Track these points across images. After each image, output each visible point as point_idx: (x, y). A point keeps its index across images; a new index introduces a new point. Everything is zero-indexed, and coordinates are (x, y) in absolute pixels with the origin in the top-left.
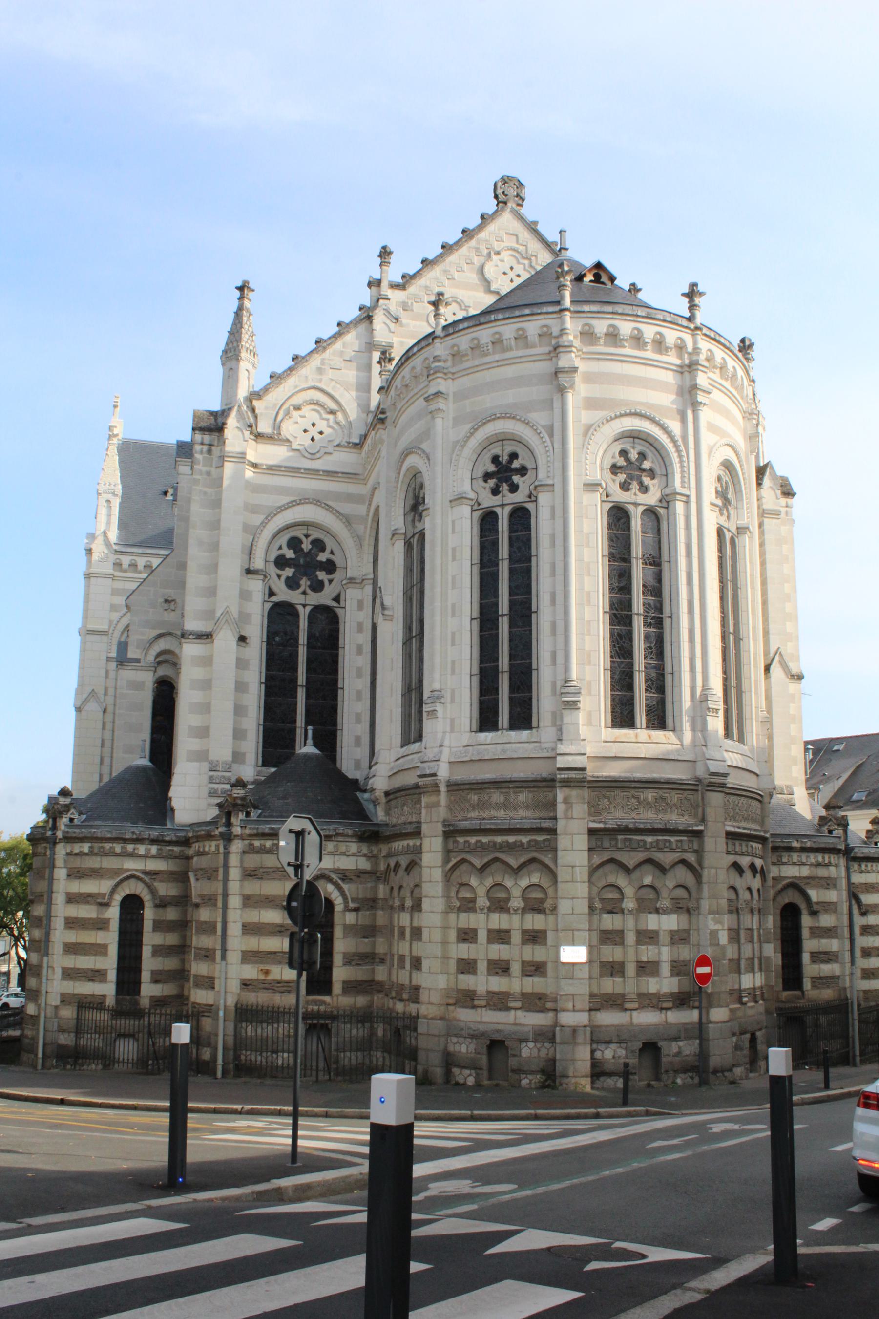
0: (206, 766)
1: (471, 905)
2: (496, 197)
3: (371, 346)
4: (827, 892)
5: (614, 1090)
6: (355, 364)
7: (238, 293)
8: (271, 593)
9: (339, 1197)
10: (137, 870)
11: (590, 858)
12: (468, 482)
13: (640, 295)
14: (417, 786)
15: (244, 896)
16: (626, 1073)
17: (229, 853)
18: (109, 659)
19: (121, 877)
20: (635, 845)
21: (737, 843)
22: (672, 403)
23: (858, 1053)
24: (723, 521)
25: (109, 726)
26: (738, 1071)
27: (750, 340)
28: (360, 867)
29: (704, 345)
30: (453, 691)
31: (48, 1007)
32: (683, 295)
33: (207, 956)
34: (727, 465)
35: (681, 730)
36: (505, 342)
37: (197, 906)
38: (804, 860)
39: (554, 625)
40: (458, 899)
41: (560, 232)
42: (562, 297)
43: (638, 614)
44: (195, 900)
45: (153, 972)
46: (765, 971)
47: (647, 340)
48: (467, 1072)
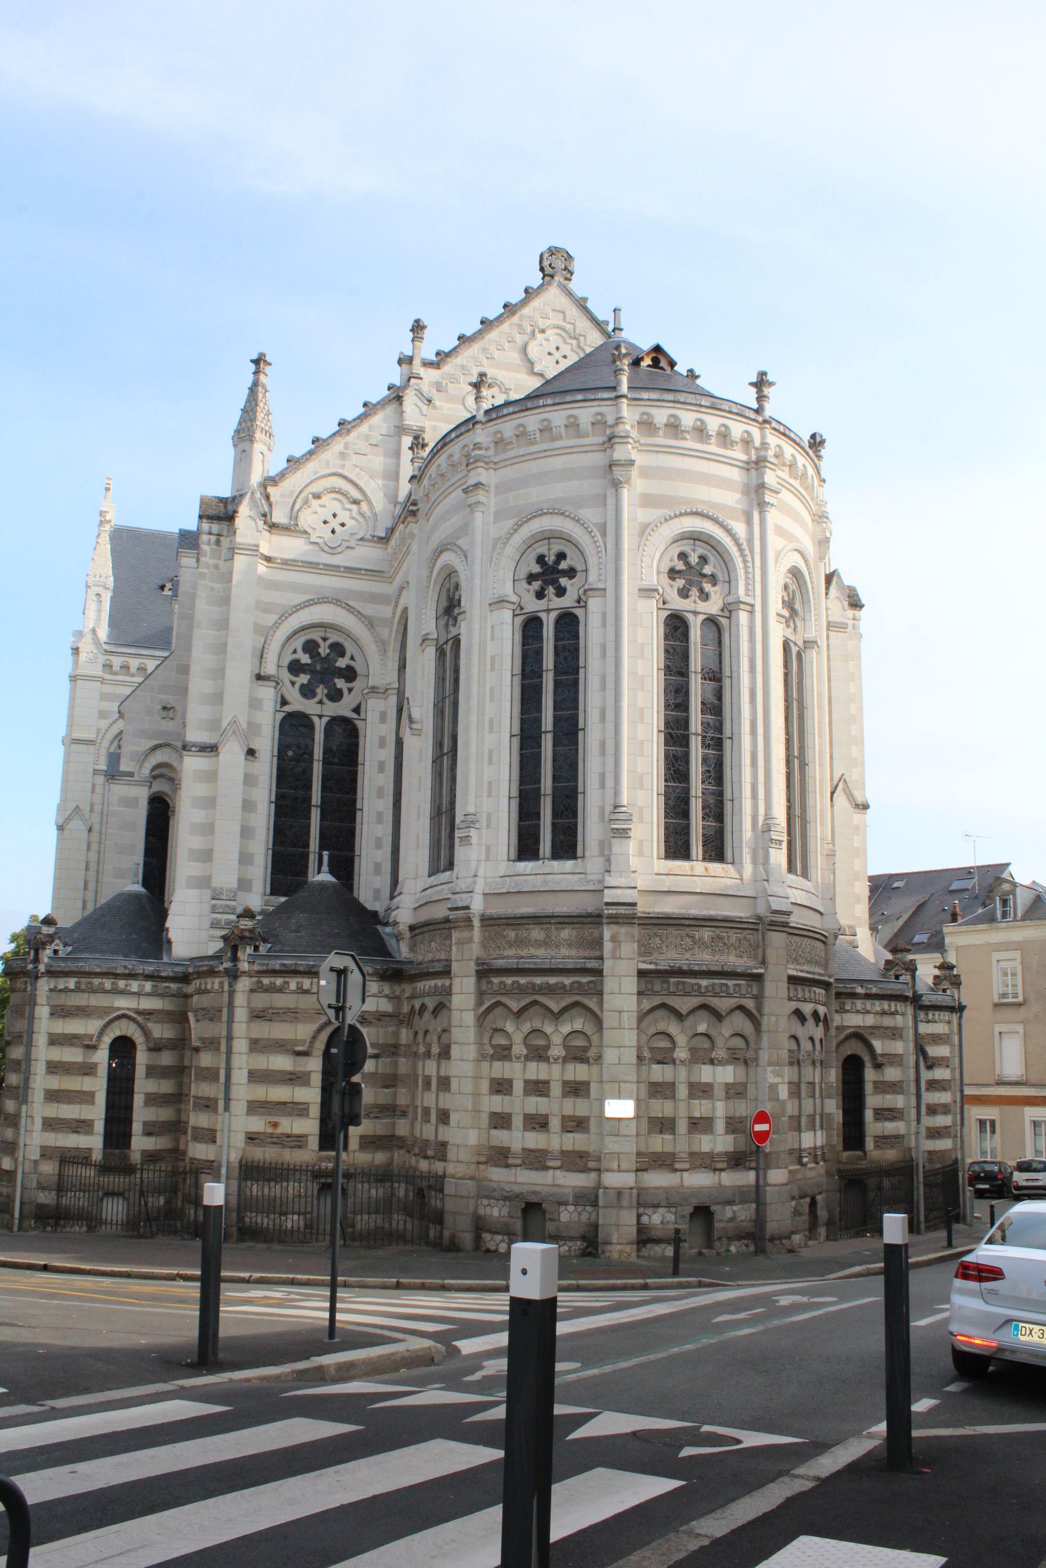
0: (207, 894)
1: (506, 1053)
2: (542, 269)
3: (401, 429)
4: (893, 1042)
5: (664, 1258)
6: (382, 450)
7: (252, 367)
8: (284, 702)
9: (386, 1376)
10: (129, 1009)
11: (639, 1003)
13: (698, 382)
14: (447, 920)
16: (677, 1240)
17: (234, 991)
18: (96, 772)
19: (111, 1017)
20: (688, 989)
21: (800, 988)
22: (737, 502)
23: (922, 1219)
24: (789, 633)
25: (95, 847)
26: (797, 1238)
27: (821, 436)
28: (381, 1009)
29: (773, 440)
30: (489, 815)
31: (27, 1162)
32: (751, 384)
33: (208, 1107)
34: (795, 573)
35: (741, 863)
36: (554, 429)
37: (197, 1050)
38: (868, 1008)
40: (491, 1045)
41: (615, 311)
42: (619, 382)
43: (696, 734)
44: (195, 1043)
45: (146, 1124)
46: (827, 1130)
47: (710, 433)
48: (499, 1238)
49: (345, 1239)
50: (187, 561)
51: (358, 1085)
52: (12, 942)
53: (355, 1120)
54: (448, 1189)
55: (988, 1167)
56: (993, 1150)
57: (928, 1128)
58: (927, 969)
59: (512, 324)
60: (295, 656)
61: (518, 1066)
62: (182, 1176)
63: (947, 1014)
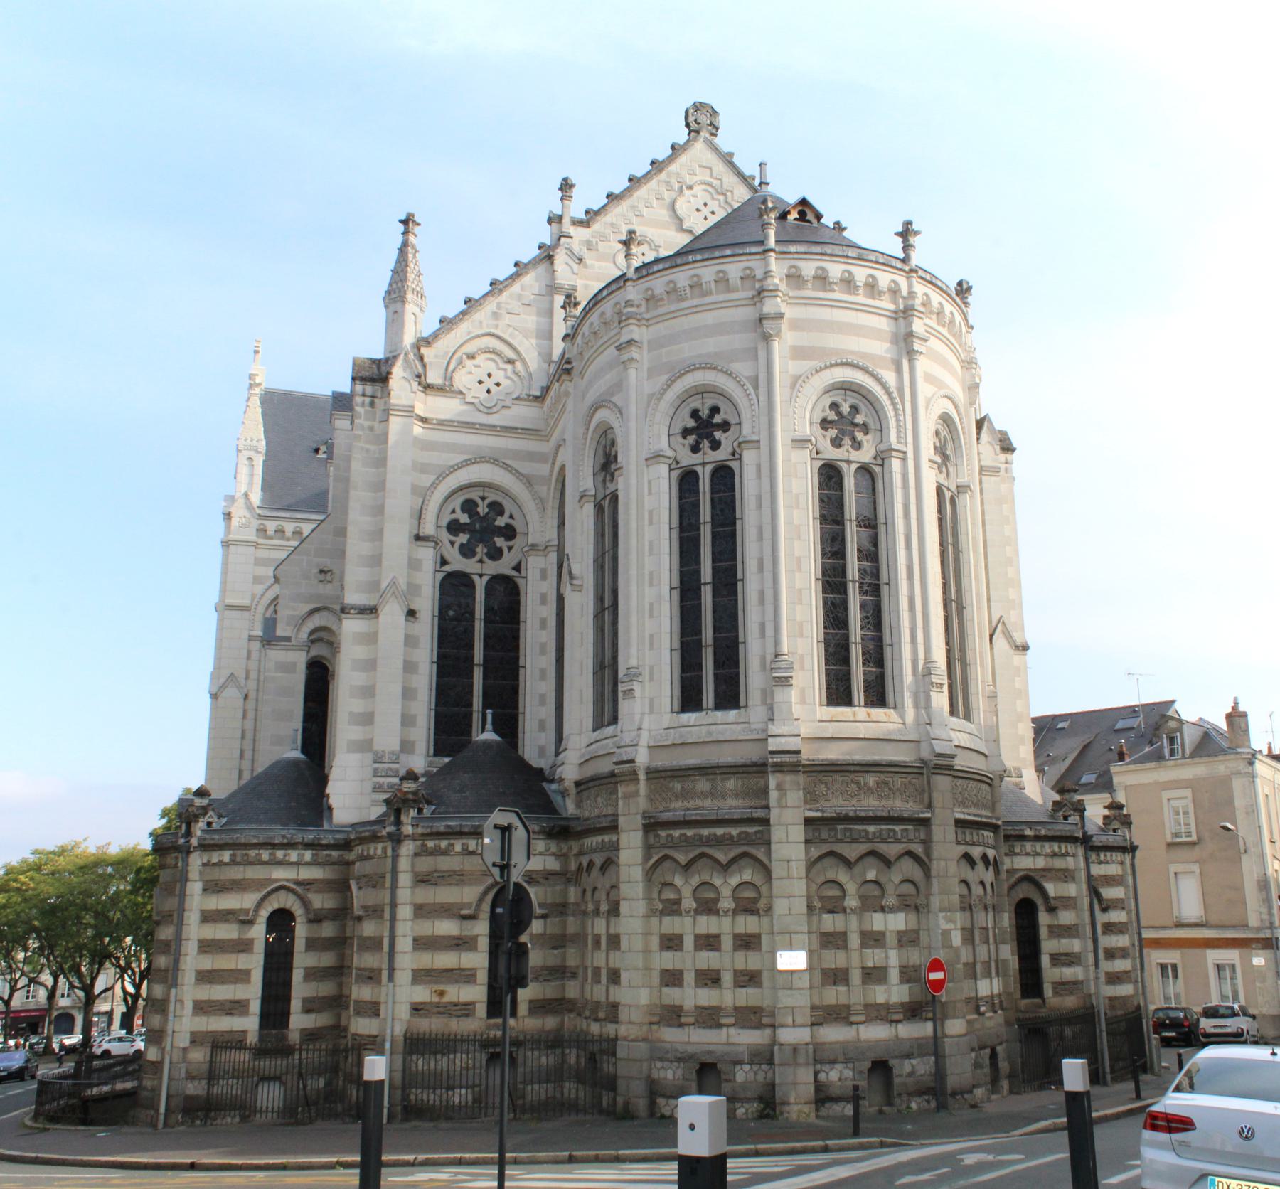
0: (369, 757)
1: (675, 907)
2: (688, 125)
3: (552, 288)
5: (843, 1118)
7: (401, 228)
8: (444, 562)
10: (287, 880)
11: (807, 852)
12: (665, 439)
13: (845, 234)
14: (612, 774)
15: (415, 905)
16: (855, 1097)
18: (251, 638)
21: (967, 831)
23: (1108, 1069)
24: (942, 479)
25: (251, 715)
26: (979, 1092)
29: (920, 289)
32: (897, 234)
33: (371, 978)
34: (946, 419)
37: (359, 919)
38: (1038, 850)
39: (762, 593)
42: (766, 237)
43: (854, 581)
44: (357, 911)
49: (515, 1111)
50: (342, 423)
51: (525, 944)
52: (163, 817)
53: (521, 981)
54: (621, 1053)
55: (1172, 1014)
56: (1177, 996)
57: (1107, 973)
58: (1095, 810)
59: (659, 181)
60: (454, 516)
61: (688, 920)
62: (342, 1051)
63: (1119, 854)
